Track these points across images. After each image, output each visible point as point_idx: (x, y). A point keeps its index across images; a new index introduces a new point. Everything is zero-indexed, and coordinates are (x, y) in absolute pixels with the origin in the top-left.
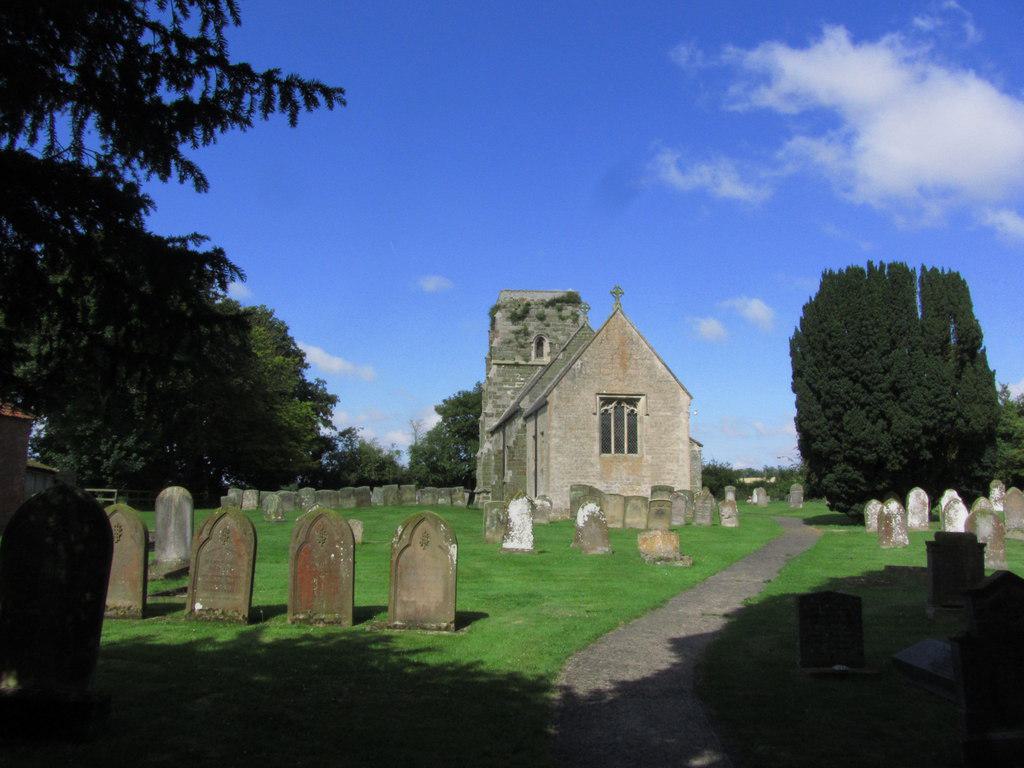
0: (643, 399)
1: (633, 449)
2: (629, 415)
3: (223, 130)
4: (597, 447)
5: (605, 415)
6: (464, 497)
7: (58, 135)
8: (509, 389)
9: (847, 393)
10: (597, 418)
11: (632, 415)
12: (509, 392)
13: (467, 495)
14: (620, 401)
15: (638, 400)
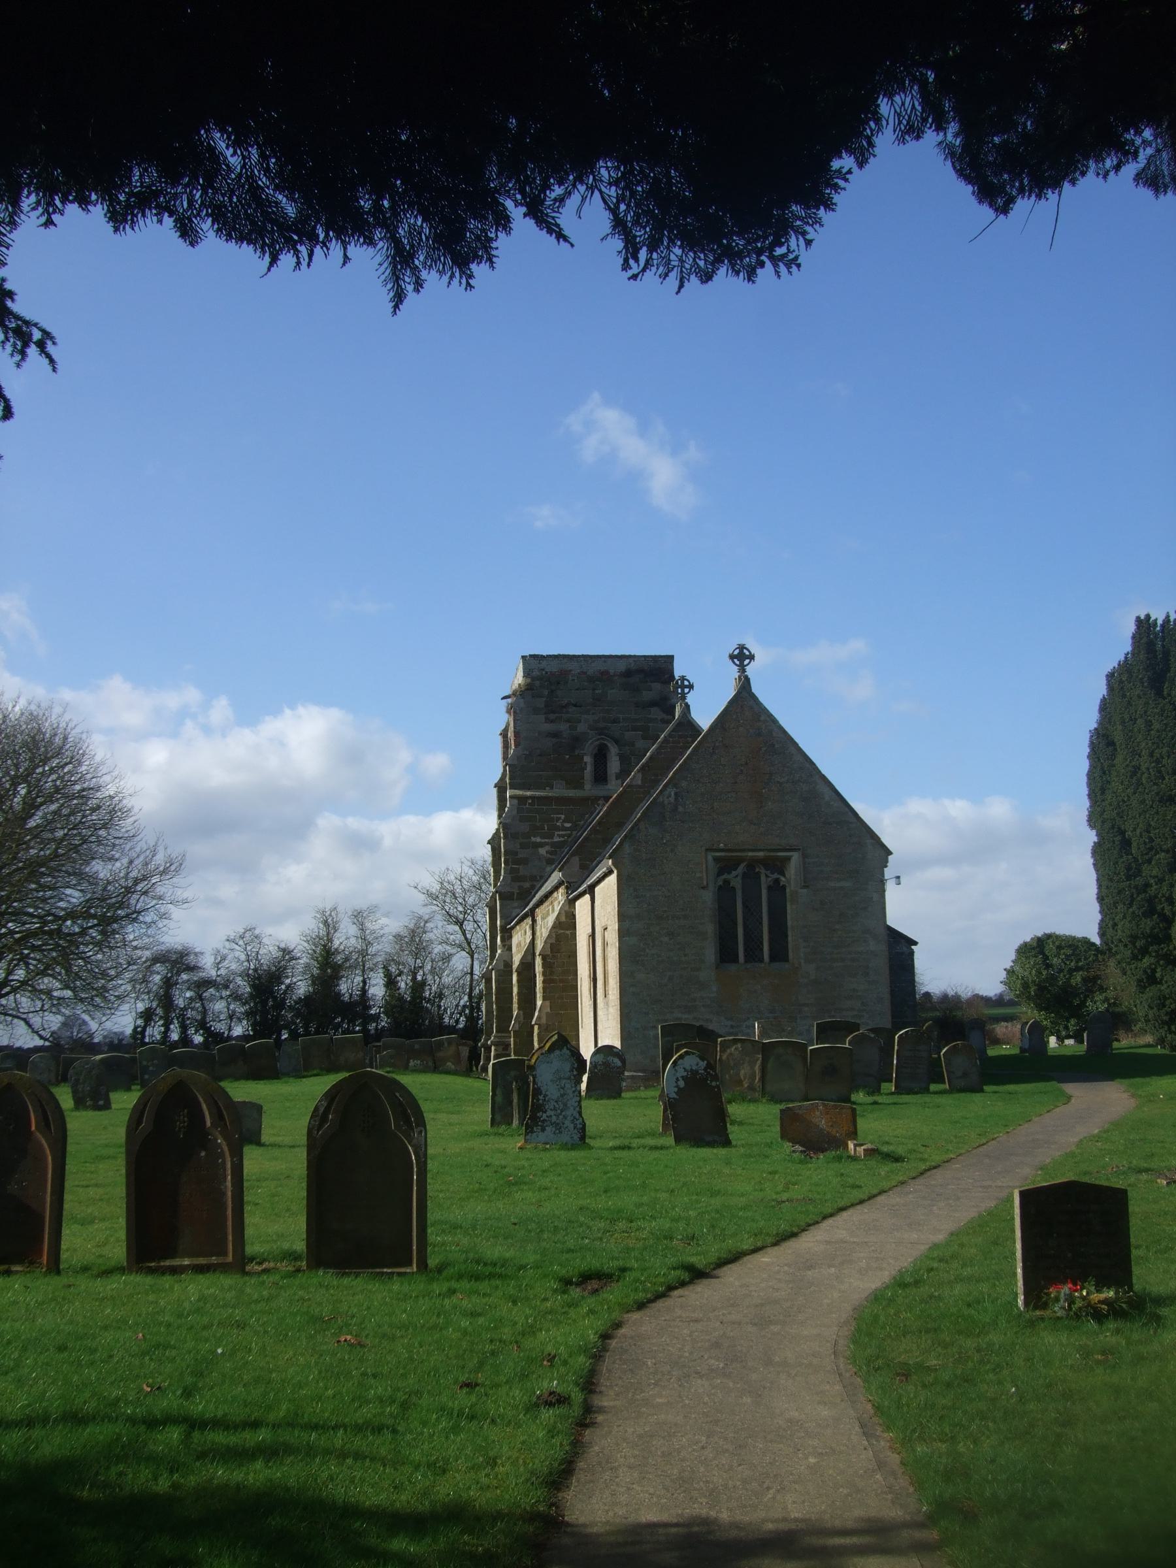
0: (795, 857)
1: (779, 954)
2: (770, 888)
3: (13, 300)
4: (710, 953)
5: (725, 892)
6: (458, 1055)
7: (19, 313)
8: (541, 845)
9: (1122, 783)
10: (708, 897)
11: (778, 889)
12: (542, 851)
13: (465, 1051)
14: (752, 864)
15: (789, 859)
